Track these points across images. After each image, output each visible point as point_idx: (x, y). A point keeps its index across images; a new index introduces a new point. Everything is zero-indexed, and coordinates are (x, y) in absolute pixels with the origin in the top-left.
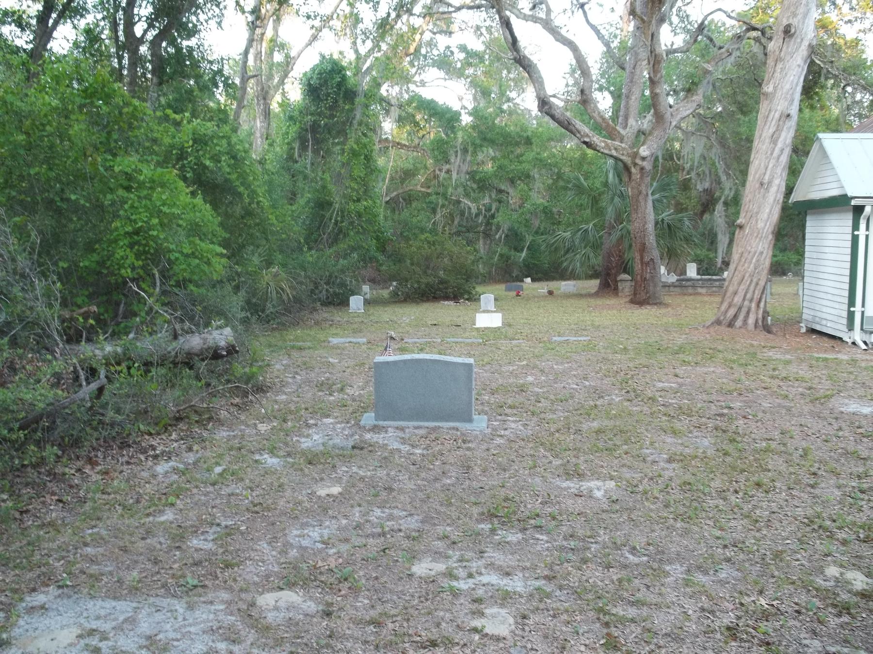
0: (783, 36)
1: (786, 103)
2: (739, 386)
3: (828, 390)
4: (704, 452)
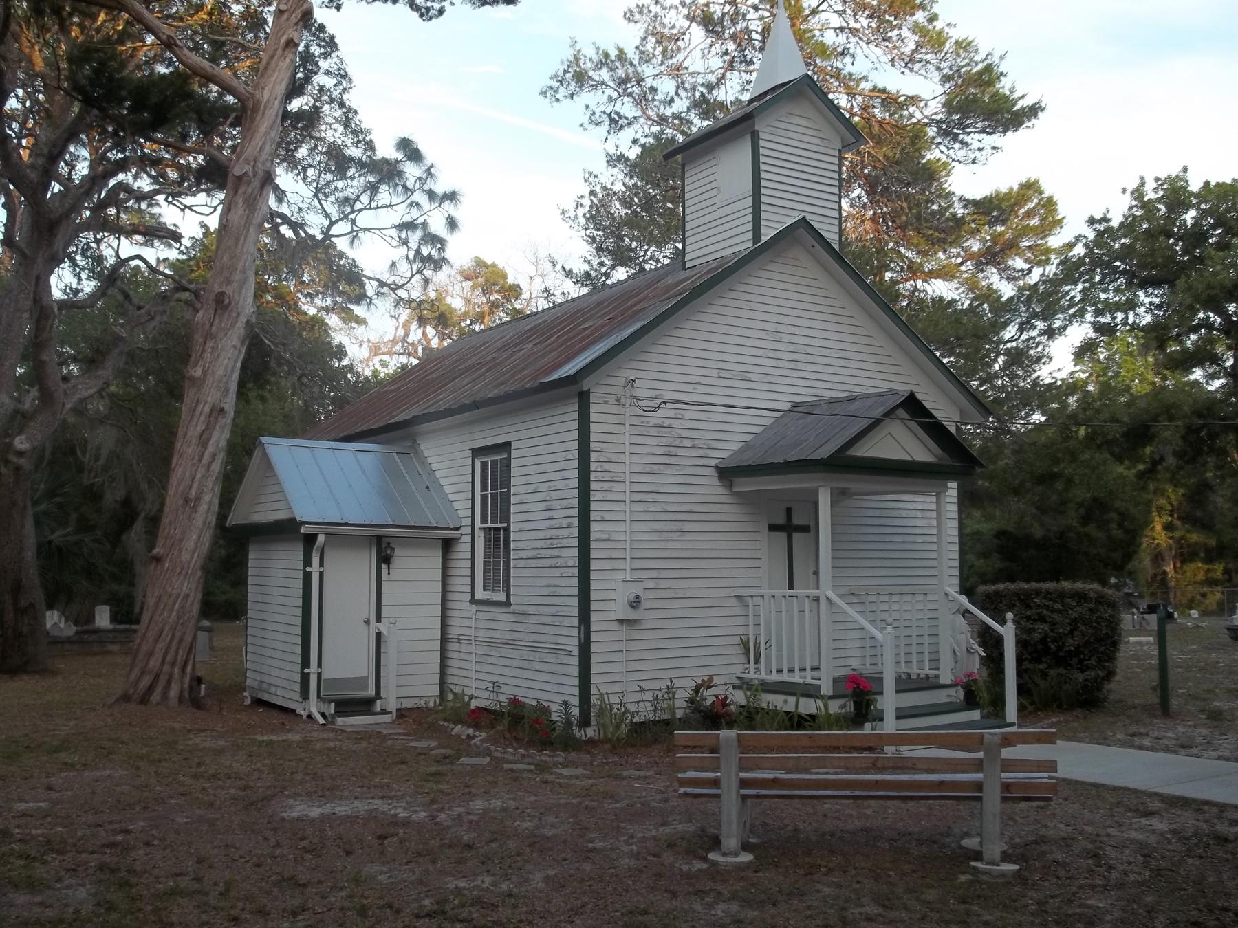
0: (214, 306)
1: (219, 394)
2: (145, 794)
3: (269, 787)
4: (77, 911)
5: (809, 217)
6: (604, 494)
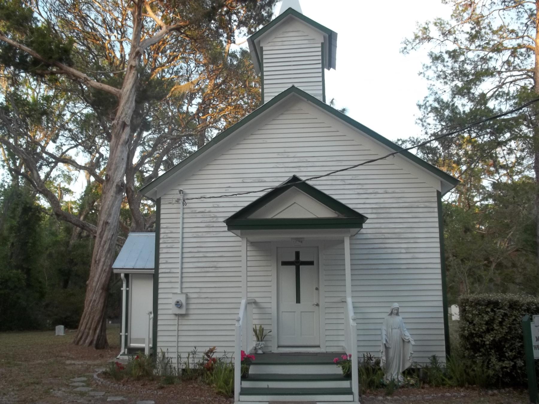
5: (296, 85)
6: (168, 249)
